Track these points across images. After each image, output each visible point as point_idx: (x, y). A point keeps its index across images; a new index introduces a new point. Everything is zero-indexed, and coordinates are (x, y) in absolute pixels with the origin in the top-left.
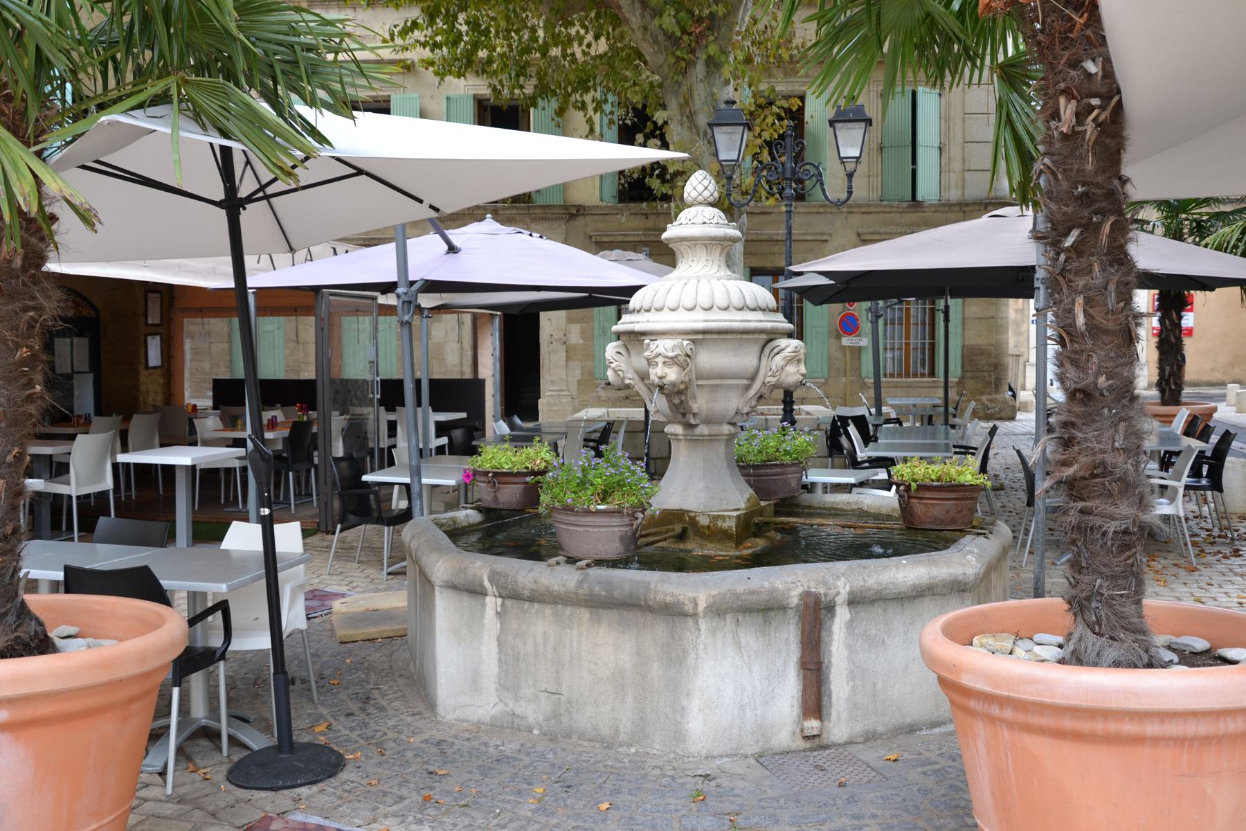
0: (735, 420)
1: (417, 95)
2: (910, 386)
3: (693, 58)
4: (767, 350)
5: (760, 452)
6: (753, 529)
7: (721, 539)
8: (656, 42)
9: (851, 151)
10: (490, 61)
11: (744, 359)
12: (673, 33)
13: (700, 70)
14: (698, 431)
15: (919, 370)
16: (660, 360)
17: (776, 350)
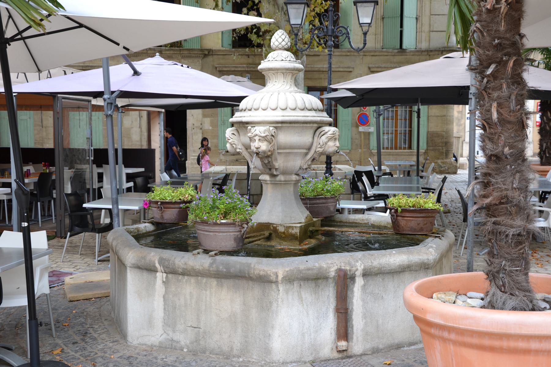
0: (299, 172)
5: (313, 191)
6: (309, 234)
7: (291, 240)
11: (303, 138)
14: (278, 178)
15: (403, 146)
16: (257, 138)
17: (322, 133)
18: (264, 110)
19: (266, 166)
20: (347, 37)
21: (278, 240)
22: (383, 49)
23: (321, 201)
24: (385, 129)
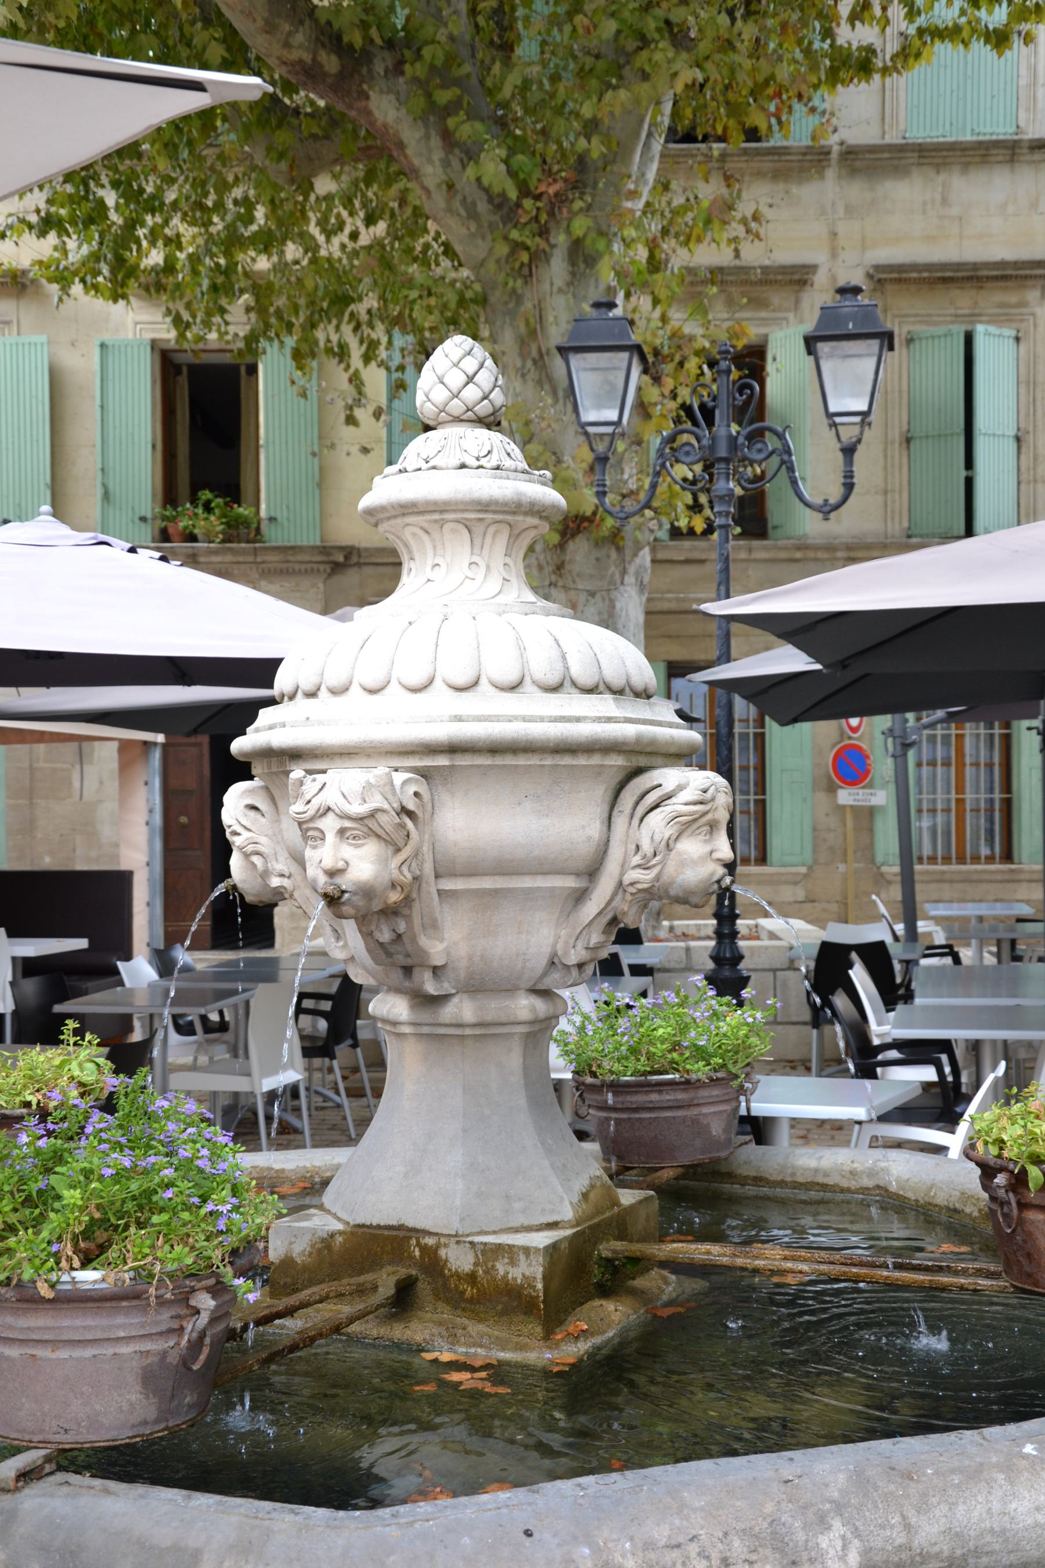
0: (546, 983)
1: (43, 338)
2: (967, 879)
3: (543, 245)
4: (628, 797)
5: (634, 1051)
6: (597, 1274)
7: (505, 1313)
8: (472, 214)
9: (848, 400)
10: (169, 267)
11: (562, 822)
12: (503, 195)
13: (557, 268)
14: (448, 1012)
15: (984, 851)
16: (330, 825)
17: (651, 798)
18: (372, 692)
19: (389, 955)
20: (783, 462)
21: (446, 1314)
22: (909, 537)
23: (668, 1097)
24: (924, 796)
